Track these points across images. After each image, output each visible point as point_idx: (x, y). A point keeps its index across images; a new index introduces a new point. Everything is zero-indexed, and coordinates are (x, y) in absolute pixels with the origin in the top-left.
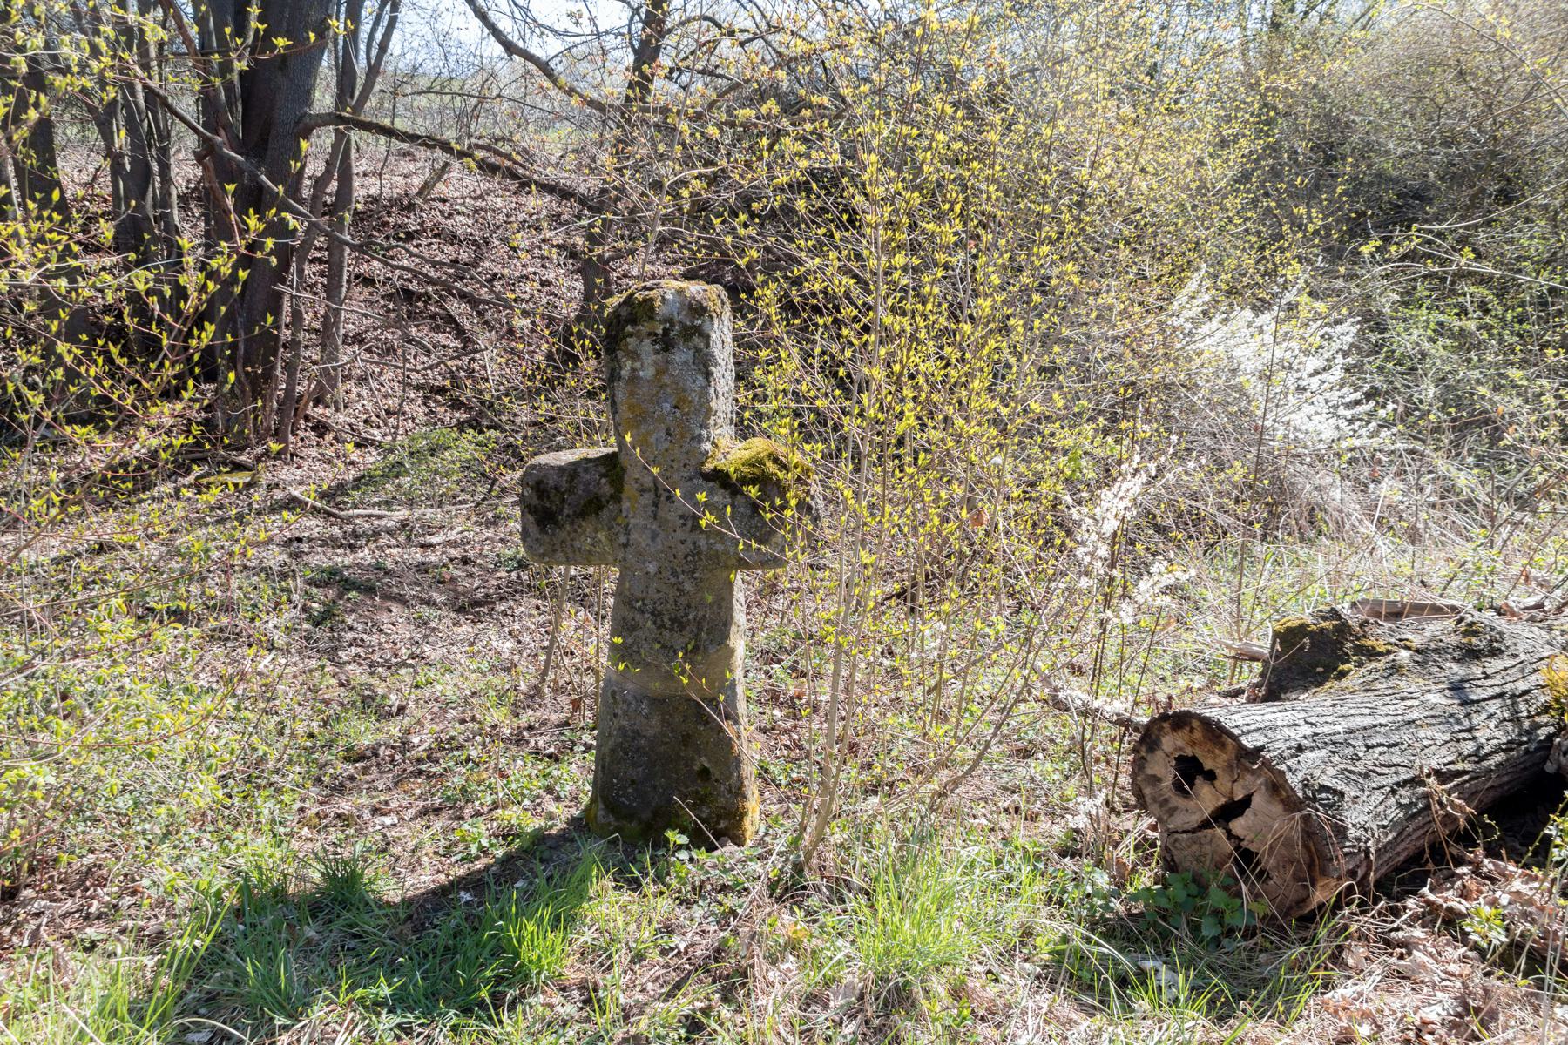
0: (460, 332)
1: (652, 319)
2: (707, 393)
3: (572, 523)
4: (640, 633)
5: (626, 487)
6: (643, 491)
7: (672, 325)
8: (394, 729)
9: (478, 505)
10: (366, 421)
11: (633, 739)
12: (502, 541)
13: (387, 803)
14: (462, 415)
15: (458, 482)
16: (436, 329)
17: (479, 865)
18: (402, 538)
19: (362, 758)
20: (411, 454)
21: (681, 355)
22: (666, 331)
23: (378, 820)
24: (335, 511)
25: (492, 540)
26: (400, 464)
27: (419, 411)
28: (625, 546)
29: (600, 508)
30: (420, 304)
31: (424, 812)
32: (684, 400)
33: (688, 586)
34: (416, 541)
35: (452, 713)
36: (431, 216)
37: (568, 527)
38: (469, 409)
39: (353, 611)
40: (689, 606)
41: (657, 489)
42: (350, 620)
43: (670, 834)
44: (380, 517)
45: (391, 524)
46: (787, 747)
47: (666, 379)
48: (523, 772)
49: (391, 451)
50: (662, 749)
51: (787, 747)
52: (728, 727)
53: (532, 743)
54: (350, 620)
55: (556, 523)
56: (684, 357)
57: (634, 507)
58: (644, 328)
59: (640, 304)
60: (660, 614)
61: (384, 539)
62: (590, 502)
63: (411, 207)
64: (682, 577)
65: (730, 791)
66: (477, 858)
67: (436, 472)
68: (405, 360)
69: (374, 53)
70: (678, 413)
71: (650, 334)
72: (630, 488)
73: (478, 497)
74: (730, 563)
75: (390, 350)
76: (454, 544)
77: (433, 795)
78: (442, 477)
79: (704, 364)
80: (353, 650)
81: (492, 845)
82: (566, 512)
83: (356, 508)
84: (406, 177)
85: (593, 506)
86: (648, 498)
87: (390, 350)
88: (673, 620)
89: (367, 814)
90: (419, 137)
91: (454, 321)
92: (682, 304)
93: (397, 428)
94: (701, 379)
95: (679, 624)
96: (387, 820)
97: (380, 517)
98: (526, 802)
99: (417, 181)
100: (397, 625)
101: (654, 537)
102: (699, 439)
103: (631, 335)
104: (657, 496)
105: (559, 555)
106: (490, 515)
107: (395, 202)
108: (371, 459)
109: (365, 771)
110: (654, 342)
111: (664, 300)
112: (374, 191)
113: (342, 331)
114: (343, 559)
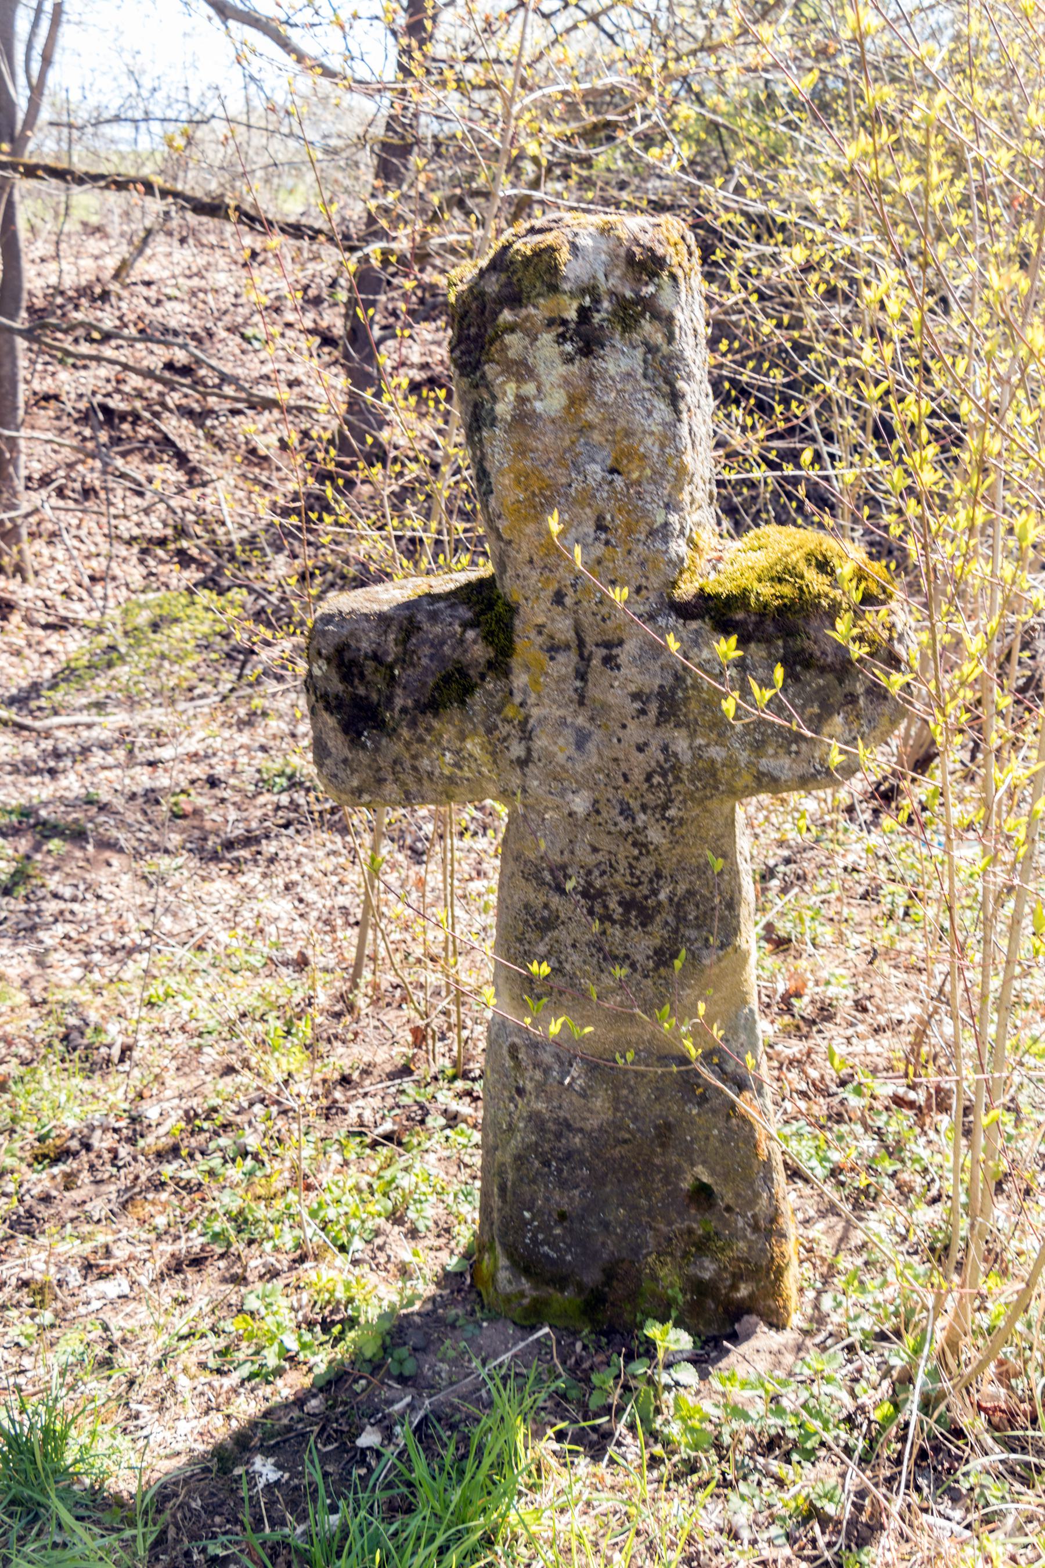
0: (182, 459)
1: (554, 289)
2: (676, 437)
3: (413, 724)
4: (560, 933)
5: (520, 644)
6: (553, 649)
7: (596, 301)
8: (115, 1092)
9: (224, 698)
10: (65, 593)
11: (559, 1136)
12: (264, 749)
13: (108, 1253)
14: (193, 575)
15: (194, 669)
16: (151, 459)
17: (287, 1387)
18: (121, 754)
19: (63, 1155)
20: (126, 634)
21: (620, 361)
22: (584, 314)
23: (97, 1289)
24: (28, 721)
25: (249, 749)
26: (112, 648)
27: (135, 574)
28: (523, 763)
29: (468, 690)
30: (126, 426)
31: (176, 1267)
32: (629, 454)
33: (655, 835)
34: (141, 756)
35: (211, 1056)
36: (133, 304)
37: (405, 733)
38: (202, 566)
39: (56, 868)
40: (658, 875)
41: (581, 644)
42: (53, 882)
43: (654, 1331)
44: (89, 726)
45: (105, 735)
46: (804, 1094)
47: (590, 414)
48: (344, 1183)
49: (100, 631)
50: (616, 1152)
51: (804, 1094)
52: (744, 1103)
53: (353, 1113)
54: (53, 882)
55: (380, 725)
56: (625, 364)
57: (538, 683)
58: (537, 311)
59: (527, 261)
60: (601, 893)
61: (97, 758)
62: (447, 679)
63: (105, 296)
64: (641, 818)
65: (756, 1228)
66: (279, 1372)
67: (163, 657)
68: (110, 504)
69: (36, 66)
70: (619, 481)
71: (551, 323)
72: (527, 645)
73: (224, 688)
74: (739, 784)
75: (88, 492)
76: (194, 757)
77: (189, 1227)
78: (172, 663)
79: (664, 375)
80: (60, 929)
81: (304, 1346)
82: (399, 702)
83: (56, 713)
84: (97, 258)
85: (453, 688)
86: (565, 663)
87: (88, 492)
88: (627, 905)
89: (74, 1277)
90: (102, 177)
91: (173, 444)
92: (613, 256)
93: (105, 598)
94: (662, 409)
95: (639, 910)
96: (112, 1288)
97: (89, 726)
98: (357, 1244)
99: (111, 263)
100: (118, 883)
101: (581, 740)
102: (664, 532)
103: (511, 329)
104: (585, 659)
105: (391, 789)
106: (242, 712)
107: (84, 291)
108: (72, 646)
109: (69, 1182)
110: (561, 339)
111: (574, 248)
112: (53, 280)
113: (23, 473)
114: (39, 791)
